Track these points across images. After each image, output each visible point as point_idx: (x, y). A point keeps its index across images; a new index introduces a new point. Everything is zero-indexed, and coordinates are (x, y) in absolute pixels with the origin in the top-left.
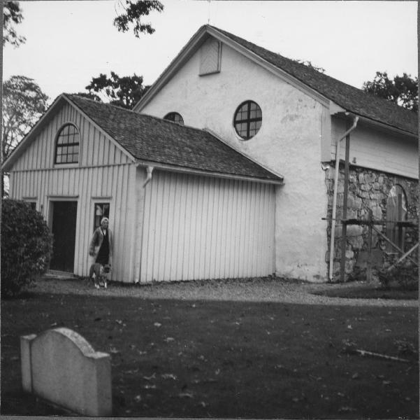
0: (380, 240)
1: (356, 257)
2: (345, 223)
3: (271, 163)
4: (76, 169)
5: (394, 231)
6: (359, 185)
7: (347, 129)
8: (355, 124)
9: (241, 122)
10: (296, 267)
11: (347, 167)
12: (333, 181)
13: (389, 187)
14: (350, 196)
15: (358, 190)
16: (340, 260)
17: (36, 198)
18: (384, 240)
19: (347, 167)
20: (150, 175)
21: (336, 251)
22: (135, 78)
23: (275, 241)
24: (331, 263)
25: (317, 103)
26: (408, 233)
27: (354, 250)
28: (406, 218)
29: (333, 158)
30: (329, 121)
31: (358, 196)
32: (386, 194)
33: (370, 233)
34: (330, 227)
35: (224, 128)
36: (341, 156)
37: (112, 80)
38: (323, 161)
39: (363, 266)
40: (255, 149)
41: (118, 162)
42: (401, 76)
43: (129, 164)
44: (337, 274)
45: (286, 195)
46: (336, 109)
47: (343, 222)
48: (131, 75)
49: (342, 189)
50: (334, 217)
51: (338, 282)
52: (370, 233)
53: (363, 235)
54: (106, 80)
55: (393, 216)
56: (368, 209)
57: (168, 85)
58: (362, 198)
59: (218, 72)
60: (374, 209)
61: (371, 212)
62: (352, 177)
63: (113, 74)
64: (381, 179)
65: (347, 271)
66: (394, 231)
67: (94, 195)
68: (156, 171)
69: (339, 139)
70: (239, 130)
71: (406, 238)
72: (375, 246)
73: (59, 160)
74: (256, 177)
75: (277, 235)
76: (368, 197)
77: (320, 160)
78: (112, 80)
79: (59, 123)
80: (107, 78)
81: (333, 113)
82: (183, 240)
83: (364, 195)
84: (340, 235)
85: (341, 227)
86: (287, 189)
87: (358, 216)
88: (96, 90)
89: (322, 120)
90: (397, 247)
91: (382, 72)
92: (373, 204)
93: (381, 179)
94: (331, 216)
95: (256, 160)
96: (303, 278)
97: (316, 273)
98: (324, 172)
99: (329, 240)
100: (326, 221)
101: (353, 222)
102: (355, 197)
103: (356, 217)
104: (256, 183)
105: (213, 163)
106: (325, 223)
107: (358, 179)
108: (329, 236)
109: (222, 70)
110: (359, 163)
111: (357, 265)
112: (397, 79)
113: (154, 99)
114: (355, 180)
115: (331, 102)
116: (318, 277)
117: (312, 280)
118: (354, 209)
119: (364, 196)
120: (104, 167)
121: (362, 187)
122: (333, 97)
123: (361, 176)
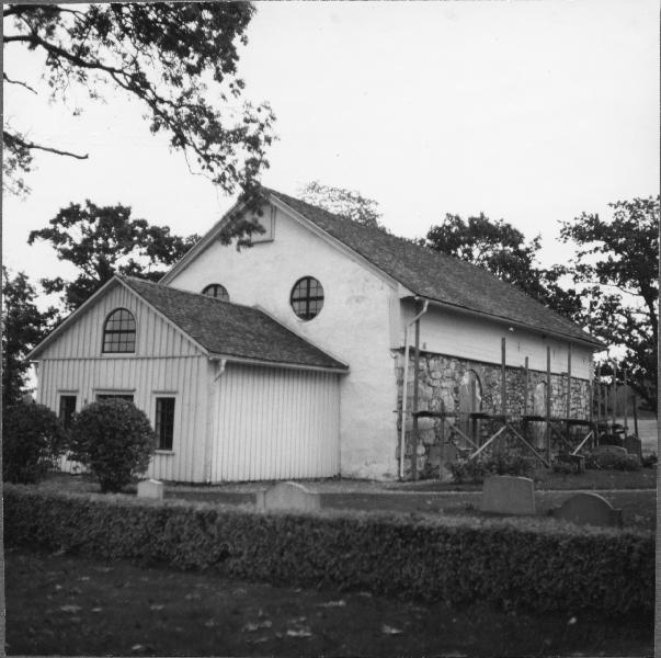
0: (453, 434)
1: (427, 453)
2: (417, 415)
3: (336, 349)
4: (131, 359)
5: (468, 422)
6: (429, 372)
7: (417, 313)
8: (425, 309)
9: (299, 300)
10: (363, 465)
12: (403, 370)
13: (462, 374)
14: (421, 386)
15: (428, 379)
16: (412, 457)
17: (77, 391)
18: (457, 433)
19: (417, 354)
20: (223, 369)
21: (407, 446)
22: (120, 209)
23: (340, 437)
24: (402, 459)
27: (426, 445)
28: (481, 408)
29: (403, 345)
30: (398, 305)
31: (429, 385)
32: (458, 382)
33: (442, 426)
34: (400, 420)
35: (280, 306)
36: (411, 343)
37: (88, 210)
39: (436, 462)
40: (314, 331)
41: (185, 353)
42: (478, 216)
43: (199, 357)
44: (407, 472)
45: (352, 384)
46: (406, 293)
47: (413, 414)
48: (114, 204)
49: (413, 378)
50: (404, 408)
51: (409, 480)
52: (442, 426)
53: (435, 428)
54: (78, 212)
55: (467, 407)
56: (439, 399)
57: (211, 249)
59: (271, 241)
60: (446, 399)
61: (443, 404)
62: (422, 364)
63: (88, 203)
64: (453, 365)
65: (418, 468)
66: (468, 422)
67: (155, 389)
68: (229, 365)
70: (297, 308)
71: (482, 431)
72: (447, 440)
73: (107, 348)
74: (320, 366)
75: (342, 430)
78: (88, 210)
79: (108, 306)
80: (81, 209)
81: (402, 297)
82: (248, 440)
83: (435, 384)
84: (411, 429)
85: (411, 420)
86: (353, 378)
88: (65, 225)
89: (390, 303)
90: (471, 441)
92: (445, 393)
93: (453, 365)
94: (401, 408)
95: (317, 345)
96: (371, 477)
97: (385, 471)
98: (393, 360)
99: (400, 435)
101: (424, 414)
103: (427, 409)
104: (320, 372)
105: (270, 349)
106: (396, 416)
108: (400, 430)
109: (276, 239)
110: (429, 349)
112: (471, 220)
113: (191, 266)
114: (425, 367)
116: (387, 475)
117: (382, 479)
118: (425, 399)
120: (167, 358)
121: (433, 375)
122: (401, 276)
123: (432, 362)
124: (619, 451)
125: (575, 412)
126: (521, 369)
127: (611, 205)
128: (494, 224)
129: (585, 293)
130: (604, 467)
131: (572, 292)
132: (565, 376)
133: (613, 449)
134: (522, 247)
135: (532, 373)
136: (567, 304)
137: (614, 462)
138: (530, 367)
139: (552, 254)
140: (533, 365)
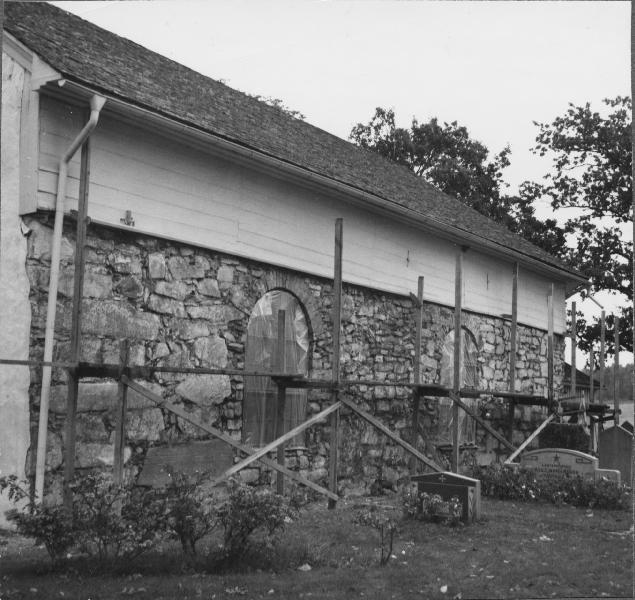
2: (83, 371)
6: (150, 282)
8: (95, 116)
11: (82, 228)
13: (253, 295)
25: (16, 65)
26: (316, 401)
29: (45, 203)
31: (147, 309)
34: (35, 387)
38: (24, 213)
46: (44, 74)
50: (48, 357)
58: (162, 315)
66: (269, 396)
69: (64, 157)
76: (183, 313)
77: (18, 213)
87: (147, 358)
91: (386, 109)
92: (197, 330)
94: (41, 356)
98: (25, 239)
100: (27, 367)
102: (134, 312)
107: (145, 267)
108: (35, 408)
111: (143, 481)
114: (136, 268)
115: (36, 58)
119: (169, 311)
124: (581, 460)
125: (528, 383)
126: (410, 298)
127: (607, 101)
128: (444, 128)
129: (570, 227)
130: (546, 498)
131: (551, 224)
132: (508, 321)
133: (568, 457)
134: (485, 164)
135: (437, 310)
136: (548, 238)
137: (567, 487)
138: (426, 296)
139: (524, 170)
140: (429, 294)
